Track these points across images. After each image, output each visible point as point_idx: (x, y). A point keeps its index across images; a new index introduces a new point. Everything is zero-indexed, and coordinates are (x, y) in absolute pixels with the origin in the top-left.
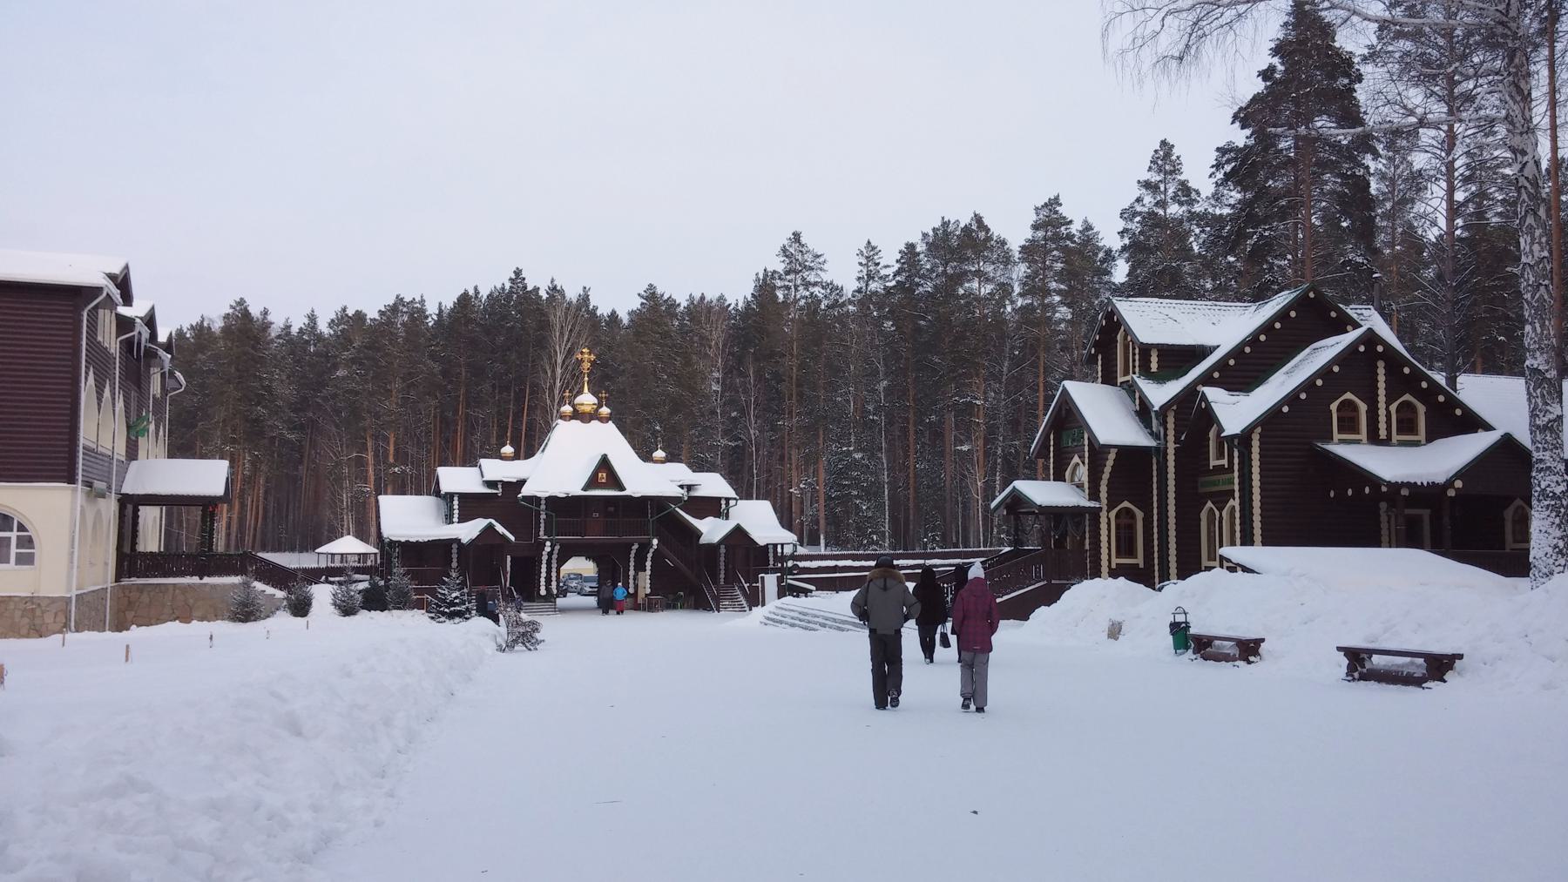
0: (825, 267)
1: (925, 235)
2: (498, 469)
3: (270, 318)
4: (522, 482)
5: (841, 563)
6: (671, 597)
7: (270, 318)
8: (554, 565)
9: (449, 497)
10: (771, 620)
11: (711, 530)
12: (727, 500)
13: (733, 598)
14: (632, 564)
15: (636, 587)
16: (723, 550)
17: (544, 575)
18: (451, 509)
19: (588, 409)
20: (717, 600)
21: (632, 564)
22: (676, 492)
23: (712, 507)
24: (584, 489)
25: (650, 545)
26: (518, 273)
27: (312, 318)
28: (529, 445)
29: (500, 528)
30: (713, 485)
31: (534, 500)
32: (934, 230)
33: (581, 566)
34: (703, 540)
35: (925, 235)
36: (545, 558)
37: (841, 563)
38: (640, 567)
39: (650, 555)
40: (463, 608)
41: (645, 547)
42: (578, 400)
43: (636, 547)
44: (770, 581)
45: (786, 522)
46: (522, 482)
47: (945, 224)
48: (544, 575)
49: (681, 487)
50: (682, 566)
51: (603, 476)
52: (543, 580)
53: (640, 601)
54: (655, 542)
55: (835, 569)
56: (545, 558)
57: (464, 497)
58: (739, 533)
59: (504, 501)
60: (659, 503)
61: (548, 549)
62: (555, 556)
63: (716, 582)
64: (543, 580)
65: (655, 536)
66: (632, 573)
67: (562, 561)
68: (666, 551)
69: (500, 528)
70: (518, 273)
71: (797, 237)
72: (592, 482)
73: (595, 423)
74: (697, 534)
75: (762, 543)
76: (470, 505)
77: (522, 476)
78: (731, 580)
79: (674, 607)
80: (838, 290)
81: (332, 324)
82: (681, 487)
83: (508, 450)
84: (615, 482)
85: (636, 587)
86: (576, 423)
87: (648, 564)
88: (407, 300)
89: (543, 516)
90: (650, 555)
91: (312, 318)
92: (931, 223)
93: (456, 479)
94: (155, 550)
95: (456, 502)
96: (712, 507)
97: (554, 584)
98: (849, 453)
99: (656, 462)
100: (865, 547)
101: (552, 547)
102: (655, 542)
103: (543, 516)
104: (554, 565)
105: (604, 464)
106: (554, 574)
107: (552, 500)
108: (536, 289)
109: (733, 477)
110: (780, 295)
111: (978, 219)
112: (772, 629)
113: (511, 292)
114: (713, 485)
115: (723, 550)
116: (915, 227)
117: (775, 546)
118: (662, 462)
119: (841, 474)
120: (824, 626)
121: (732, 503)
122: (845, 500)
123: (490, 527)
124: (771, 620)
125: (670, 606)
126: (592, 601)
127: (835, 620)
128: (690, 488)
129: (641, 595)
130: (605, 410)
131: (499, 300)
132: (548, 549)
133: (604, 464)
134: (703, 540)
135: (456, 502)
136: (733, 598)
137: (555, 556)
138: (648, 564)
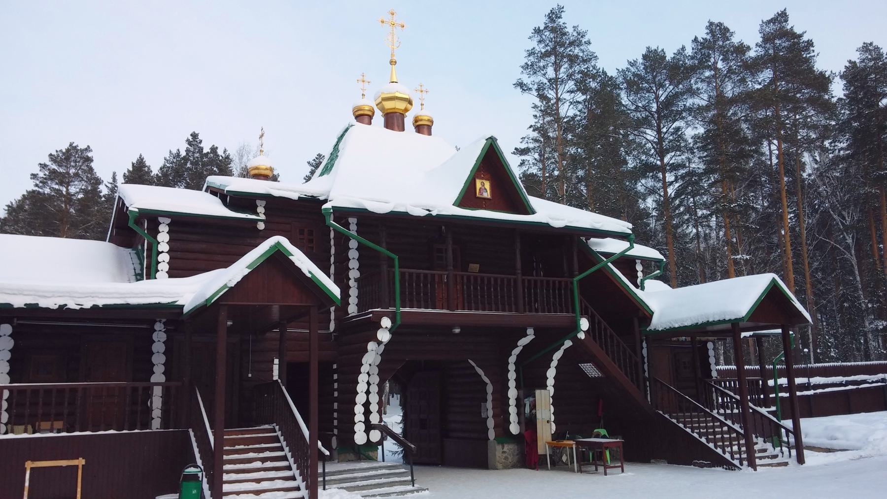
26: (195, 136)
38: (531, 382)
51: (484, 188)
55: (242, 433)
70: (195, 136)
95: (163, 237)
123: (278, 257)
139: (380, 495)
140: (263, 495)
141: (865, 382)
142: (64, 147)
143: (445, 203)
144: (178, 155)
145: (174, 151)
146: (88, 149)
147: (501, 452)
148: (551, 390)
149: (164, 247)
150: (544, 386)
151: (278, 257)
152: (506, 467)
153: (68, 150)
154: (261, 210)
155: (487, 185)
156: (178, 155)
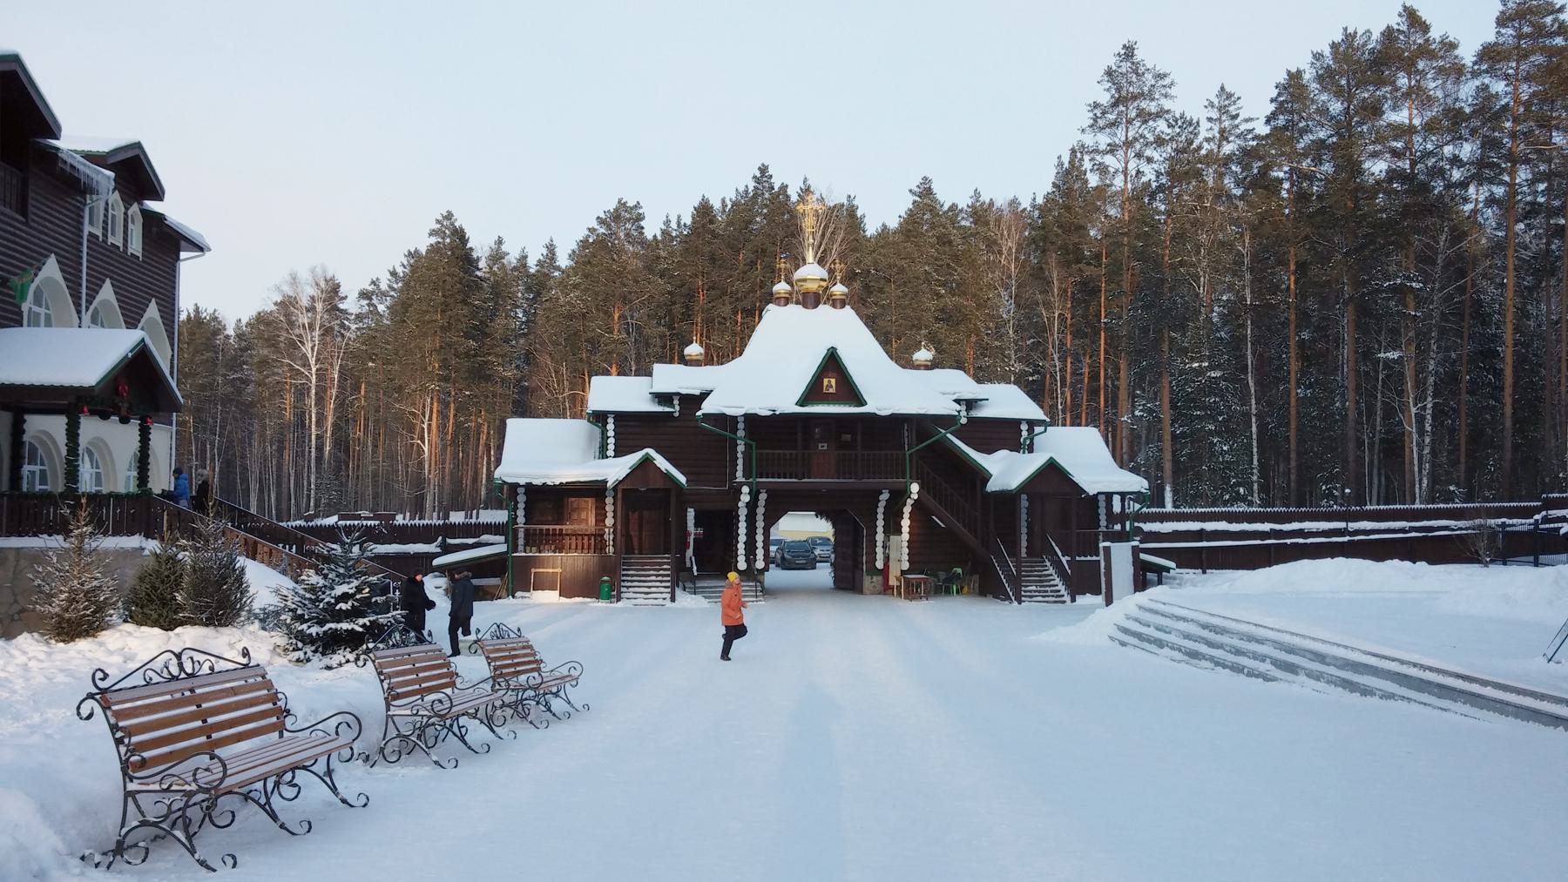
0: (1172, 92)
1: (1318, 56)
2: (671, 377)
3: (504, 248)
4: (705, 395)
5: (1210, 526)
6: (942, 575)
7: (504, 248)
8: (760, 524)
9: (599, 418)
10: (1131, 635)
11: (1006, 470)
12: (1032, 424)
13: (1042, 581)
14: (880, 523)
15: (887, 559)
16: (1024, 503)
17: (742, 538)
18: (604, 437)
19: (813, 286)
20: (1017, 583)
21: (880, 523)
22: (947, 407)
23: (1005, 434)
24: (802, 402)
25: (905, 493)
26: (763, 170)
27: (551, 249)
28: (726, 348)
29: (662, 463)
30: (1006, 401)
31: (724, 421)
32: (1334, 46)
33: (801, 526)
34: (992, 486)
35: (1318, 56)
36: (743, 512)
37: (1210, 526)
38: (893, 528)
39: (907, 510)
40: (357, 626)
41: (899, 496)
42: (799, 274)
43: (885, 496)
44: (1121, 556)
45: (1124, 459)
46: (705, 395)
47: (1349, 37)
48: (742, 538)
49: (958, 401)
50: (958, 526)
51: (830, 383)
52: (741, 547)
53: (893, 582)
54: (915, 488)
55: (1200, 535)
56: (743, 512)
57: (621, 417)
58: (1052, 470)
59: (677, 425)
60: (922, 425)
61: (745, 498)
62: (761, 510)
63: (1014, 552)
64: (741, 547)
65: (918, 478)
66: (880, 537)
67: (772, 519)
68: (931, 502)
69: (662, 463)
70: (763, 170)
71: (1129, 52)
72: (813, 393)
73: (824, 310)
74: (984, 477)
75: (1091, 490)
76: (629, 430)
77: (707, 386)
78: (1039, 550)
79: (948, 592)
80: (1189, 124)
81: (573, 255)
82: (958, 401)
83: (694, 350)
84: (850, 392)
85: (887, 559)
86: (794, 309)
87: (906, 523)
88: (630, 204)
89: (741, 448)
90: (907, 510)
91: (551, 249)
92: (1324, 38)
93: (617, 392)
94: (121, 490)
95: (611, 427)
96: (1005, 434)
97: (760, 553)
98: (1200, 372)
99: (918, 367)
100: (1231, 502)
101: (754, 496)
102: (915, 488)
103: (741, 448)
104: (760, 524)
105: (832, 363)
106: (760, 538)
107: (753, 421)
108: (784, 188)
109: (1036, 392)
110: (1093, 180)
111: (1411, 16)
112: (1136, 655)
113: (755, 196)
114: (1006, 401)
115: (1024, 503)
116: (1301, 46)
117: (1109, 496)
118: (927, 368)
119: (1192, 401)
120: (1292, 669)
121: (1037, 429)
122: (1196, 437)
123: (647, 461)
124: (1131, 635)
125: (942, 589)
126: (823, 574)
127: (1320, 658)
128: (971, 404)
129: (894, 572)
130: (839, 289)
131: (743, 209)
132: (745, 498)
133: (832, 363)
134: (992, 486)
135: (611, 427)
136: (1042, 581)
137: (761, 510)
138: (906, 523)
139: (1353, 676)
140: (1391, 702)
141: (1446, 528)
142: (612, 206)
143: (787, 403)
144: (746, 192)
145: (742, 189)
146: (638, 205)
147: (868, 582)
148: (905, 536)
149: (611, 433)
150: (900, 533)
151: (647, 461)
152: (873, 594)
153: (616, 210)
154: (676, 402)
155: (833, 381)
156: (746, 192)
